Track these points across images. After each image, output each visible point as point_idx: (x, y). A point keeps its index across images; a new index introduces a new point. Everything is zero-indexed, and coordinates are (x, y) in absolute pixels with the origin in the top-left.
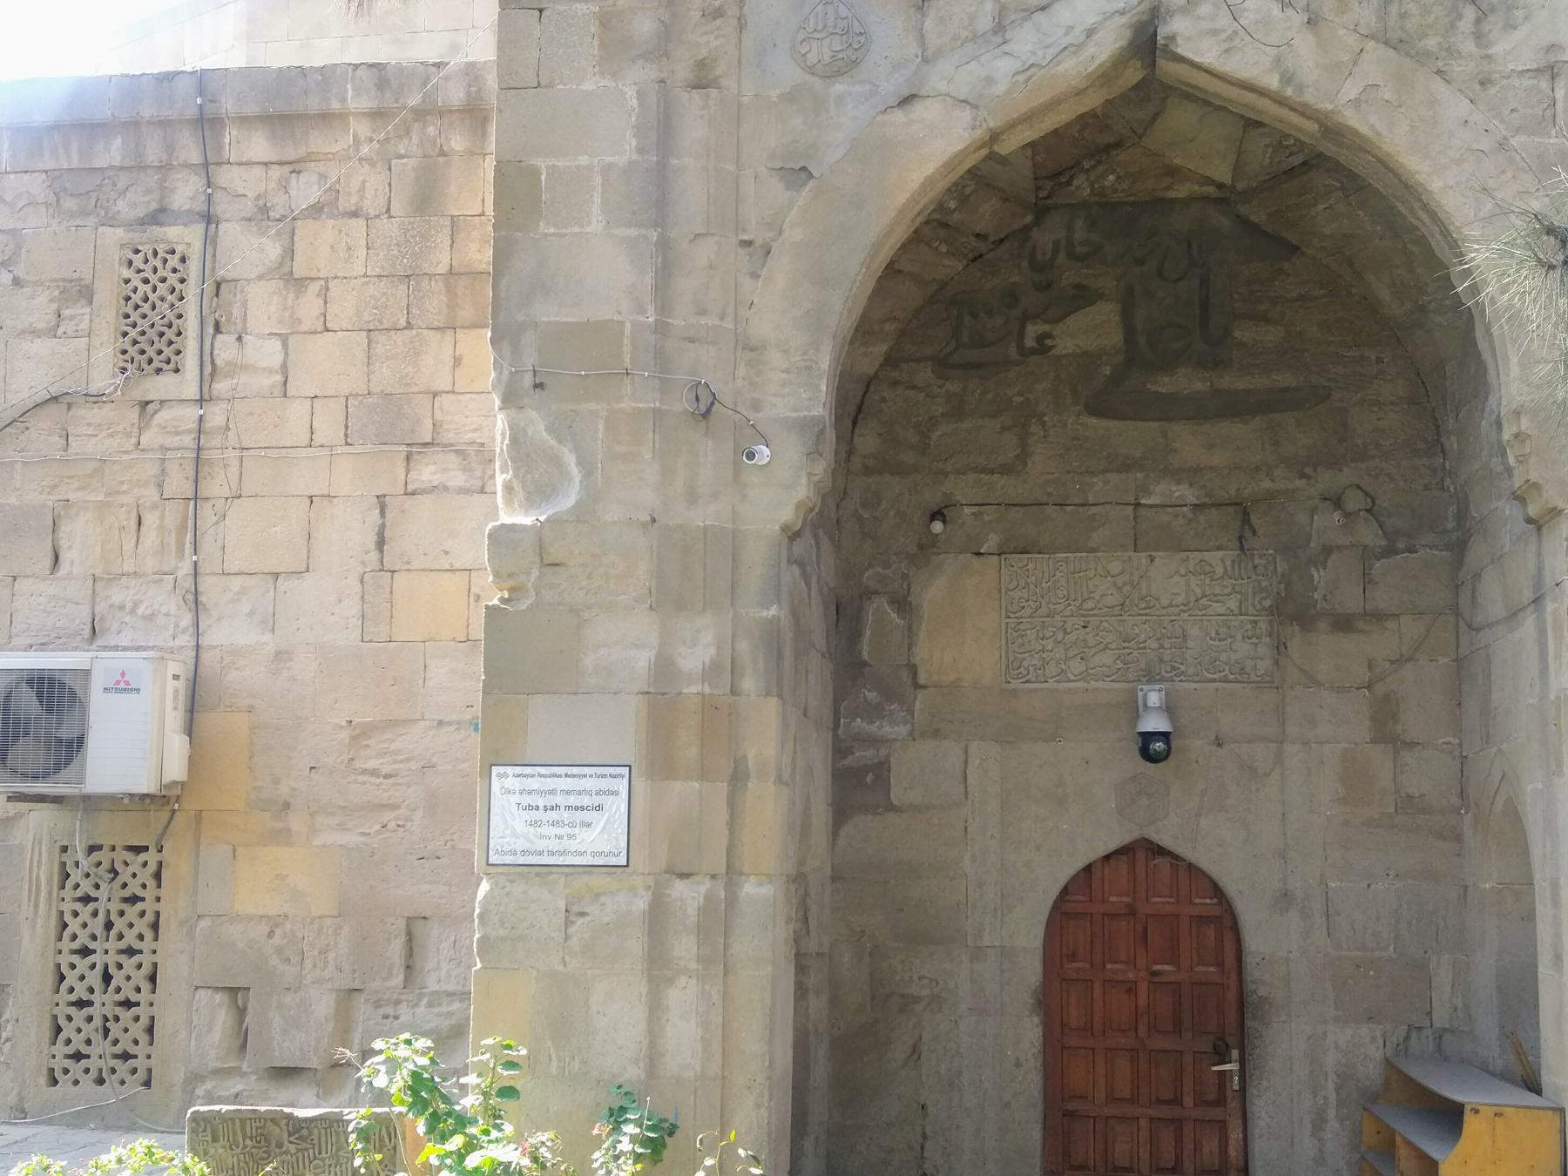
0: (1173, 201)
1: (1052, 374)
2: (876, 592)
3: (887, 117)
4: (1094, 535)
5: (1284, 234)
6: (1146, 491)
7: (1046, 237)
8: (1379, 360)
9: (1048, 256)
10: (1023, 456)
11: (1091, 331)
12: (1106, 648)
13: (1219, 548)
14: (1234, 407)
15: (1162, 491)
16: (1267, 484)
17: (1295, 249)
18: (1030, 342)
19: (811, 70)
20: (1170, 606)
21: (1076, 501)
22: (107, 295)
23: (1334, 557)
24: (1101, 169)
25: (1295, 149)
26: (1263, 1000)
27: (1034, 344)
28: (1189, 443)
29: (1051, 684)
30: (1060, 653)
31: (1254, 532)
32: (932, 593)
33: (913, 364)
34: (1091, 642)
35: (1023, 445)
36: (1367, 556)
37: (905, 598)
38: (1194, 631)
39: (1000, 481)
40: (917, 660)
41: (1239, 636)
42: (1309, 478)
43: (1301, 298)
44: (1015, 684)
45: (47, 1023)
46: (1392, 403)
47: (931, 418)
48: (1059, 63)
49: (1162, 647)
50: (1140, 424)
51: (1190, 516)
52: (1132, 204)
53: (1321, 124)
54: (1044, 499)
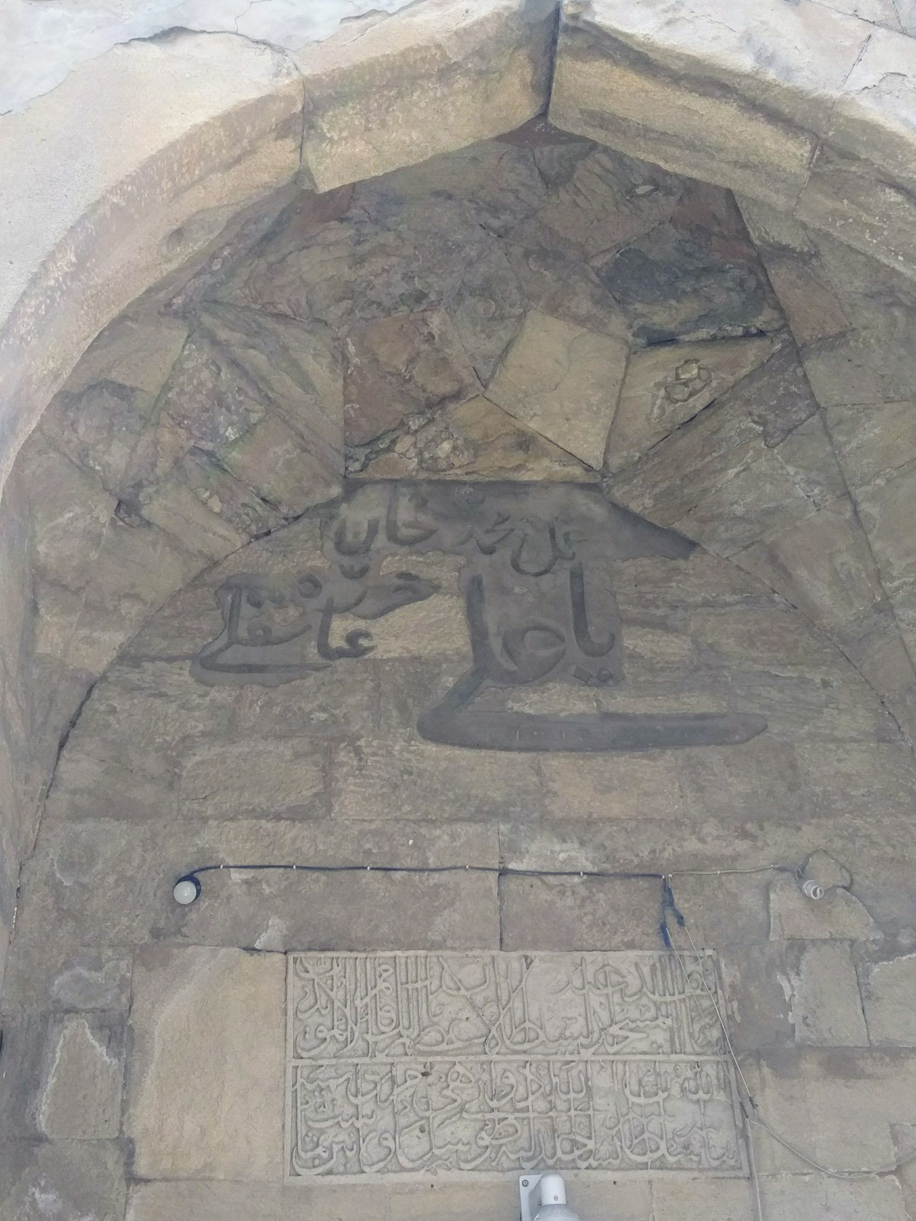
0: (527, 484)
1: (369, 685)
2: (71, 1010)
3: (128, 51)
4: (438, 920)
5: (677, 525)
6: (513, 849)
7: (360, 514)
8: (826, 684)
9: (363, 536)
10: (327, 796)
11: (426, 632)
12: (462, 1109)
13: (630, 945)
14: (638, 737)
15: (539, 851)
16: (692, 845)
17: (692, 545)
18: (336, 641)
20: (562, 1036)
21: (408, 863)
23: (808, 956)
24: (432, 430)
25: (698, 384)
27: (343, 644)
28: (573, 783)
30: (385, 1121)
31: (681, 920)
32: (169, 1013)
33: (161, 664)
34: (436, 1100)
35: (327, 774)
36: (860, 957)
37: (122, 1021)
38: (602, 1081)
39: (289, 832)
40: (135, 1131)
41: (675, 1090)
42: (754, 838)
43: (706, 604)
44: (308, 1177)
46: (854, 740)
47: (185, 738)
48: (414, 15)
49: (553, 1107)
50: (503, 754)
51: (583, 892)
52: (474, 484)
53: (820, 145)
54: (358, 860)
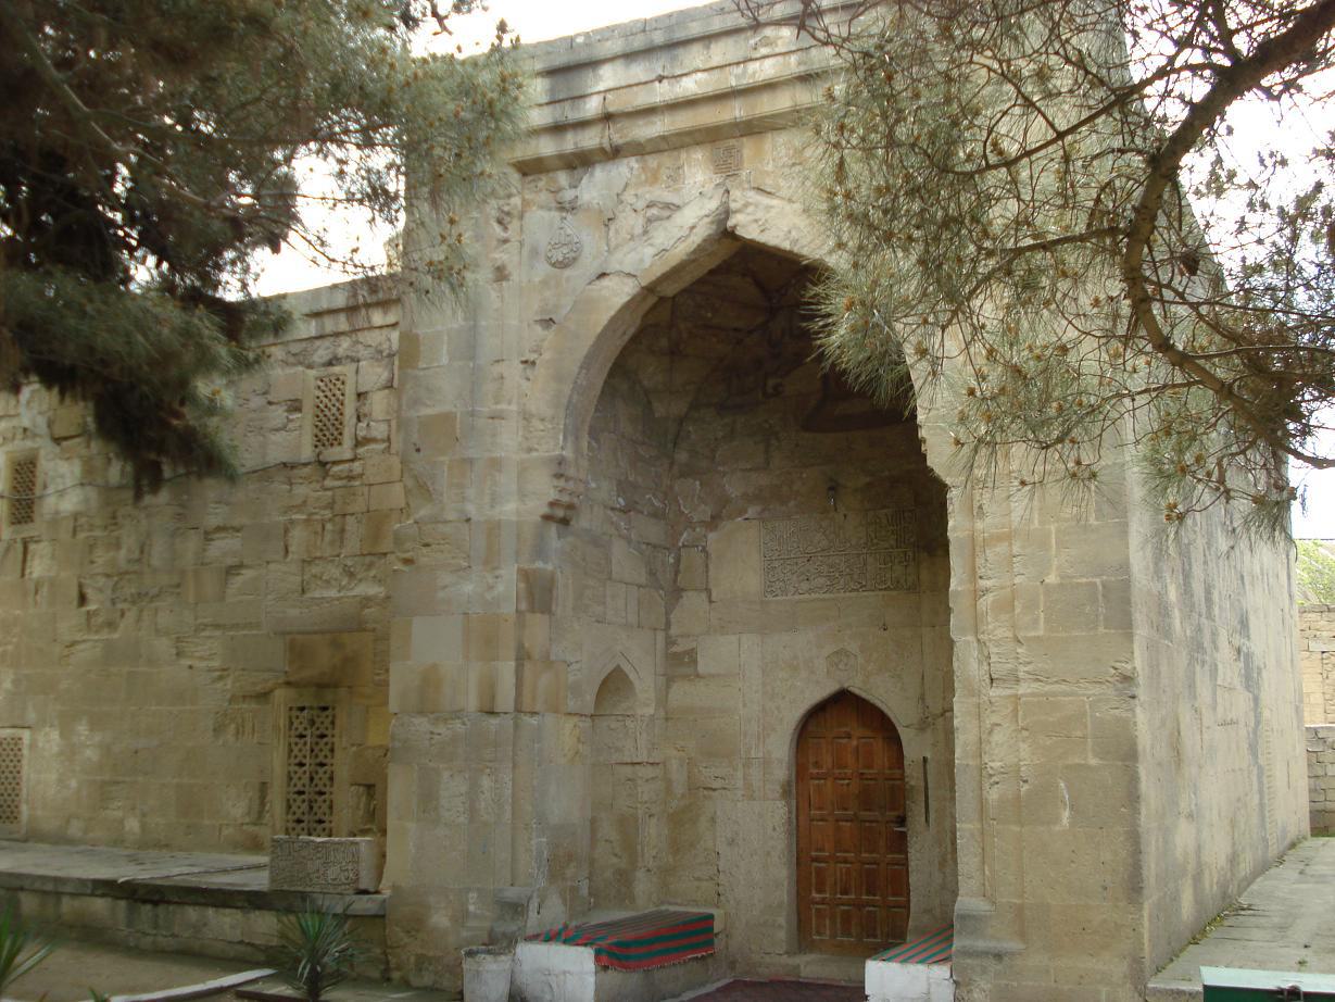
18: (770, 391)
19: (553, 265)
22: (308, 406)
26: (912, 787)
29: (790, 597)
45: (284, 805)
